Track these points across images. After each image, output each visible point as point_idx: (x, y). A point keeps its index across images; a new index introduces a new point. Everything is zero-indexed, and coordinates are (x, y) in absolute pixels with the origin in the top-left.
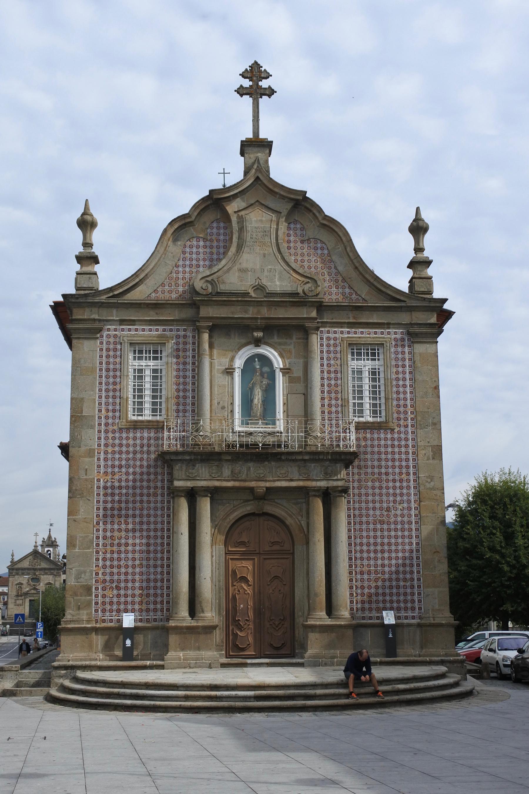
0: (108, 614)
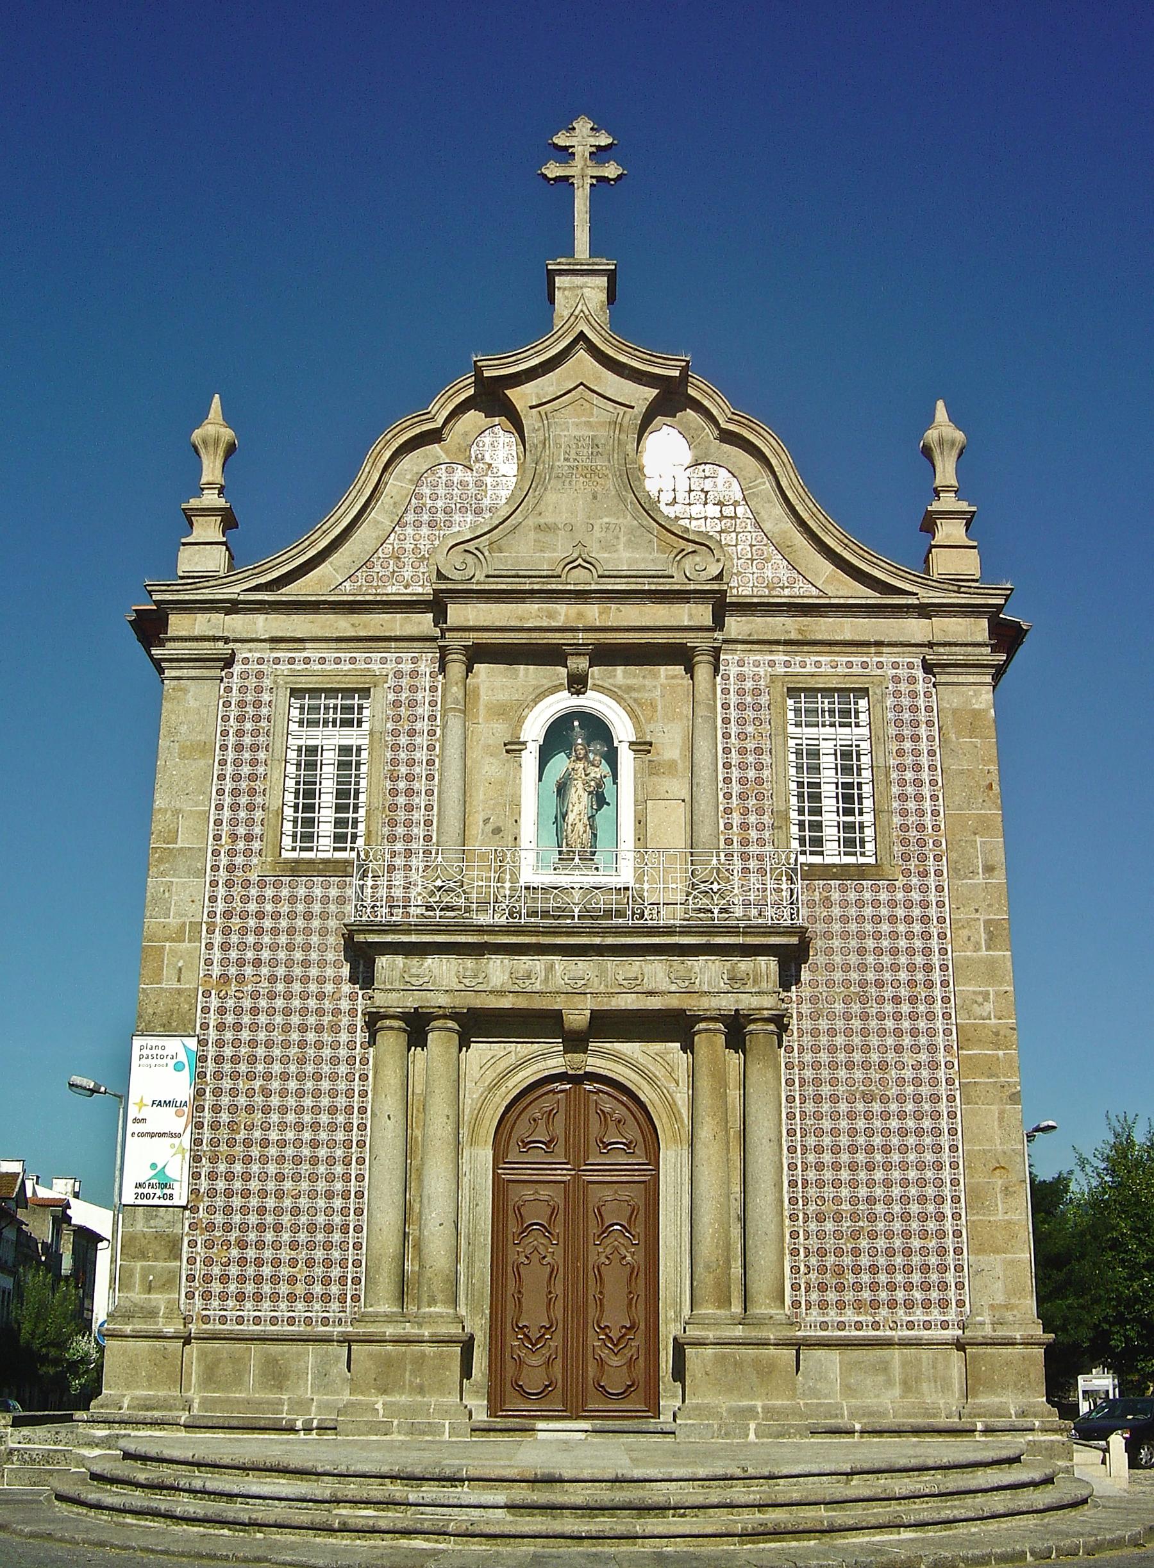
0: (215, 1303)
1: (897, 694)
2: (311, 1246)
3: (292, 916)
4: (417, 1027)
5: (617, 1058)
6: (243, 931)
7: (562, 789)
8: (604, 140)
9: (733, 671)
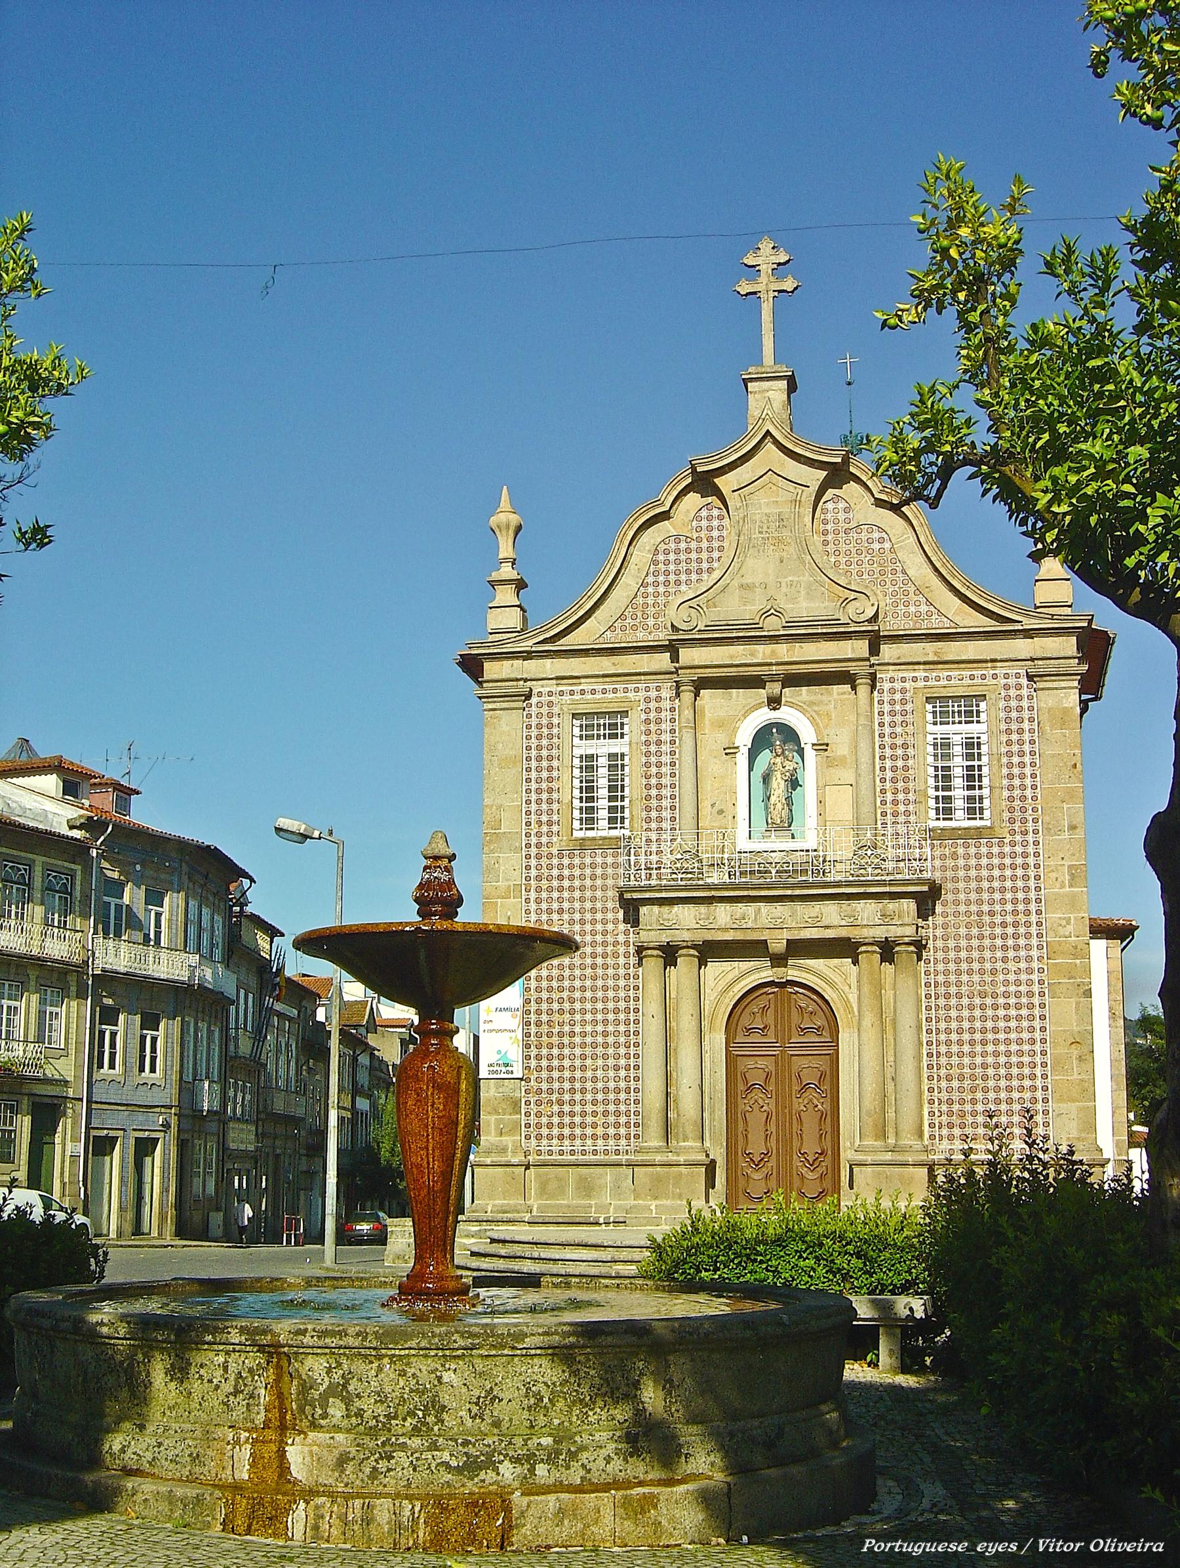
1: (1007, 698)
3: (582, 877)
4: (669, 953)
5: (808, 970)
6: (550, 889)
7: (766, 779)
8: (783, 258)
9: (887, 686)
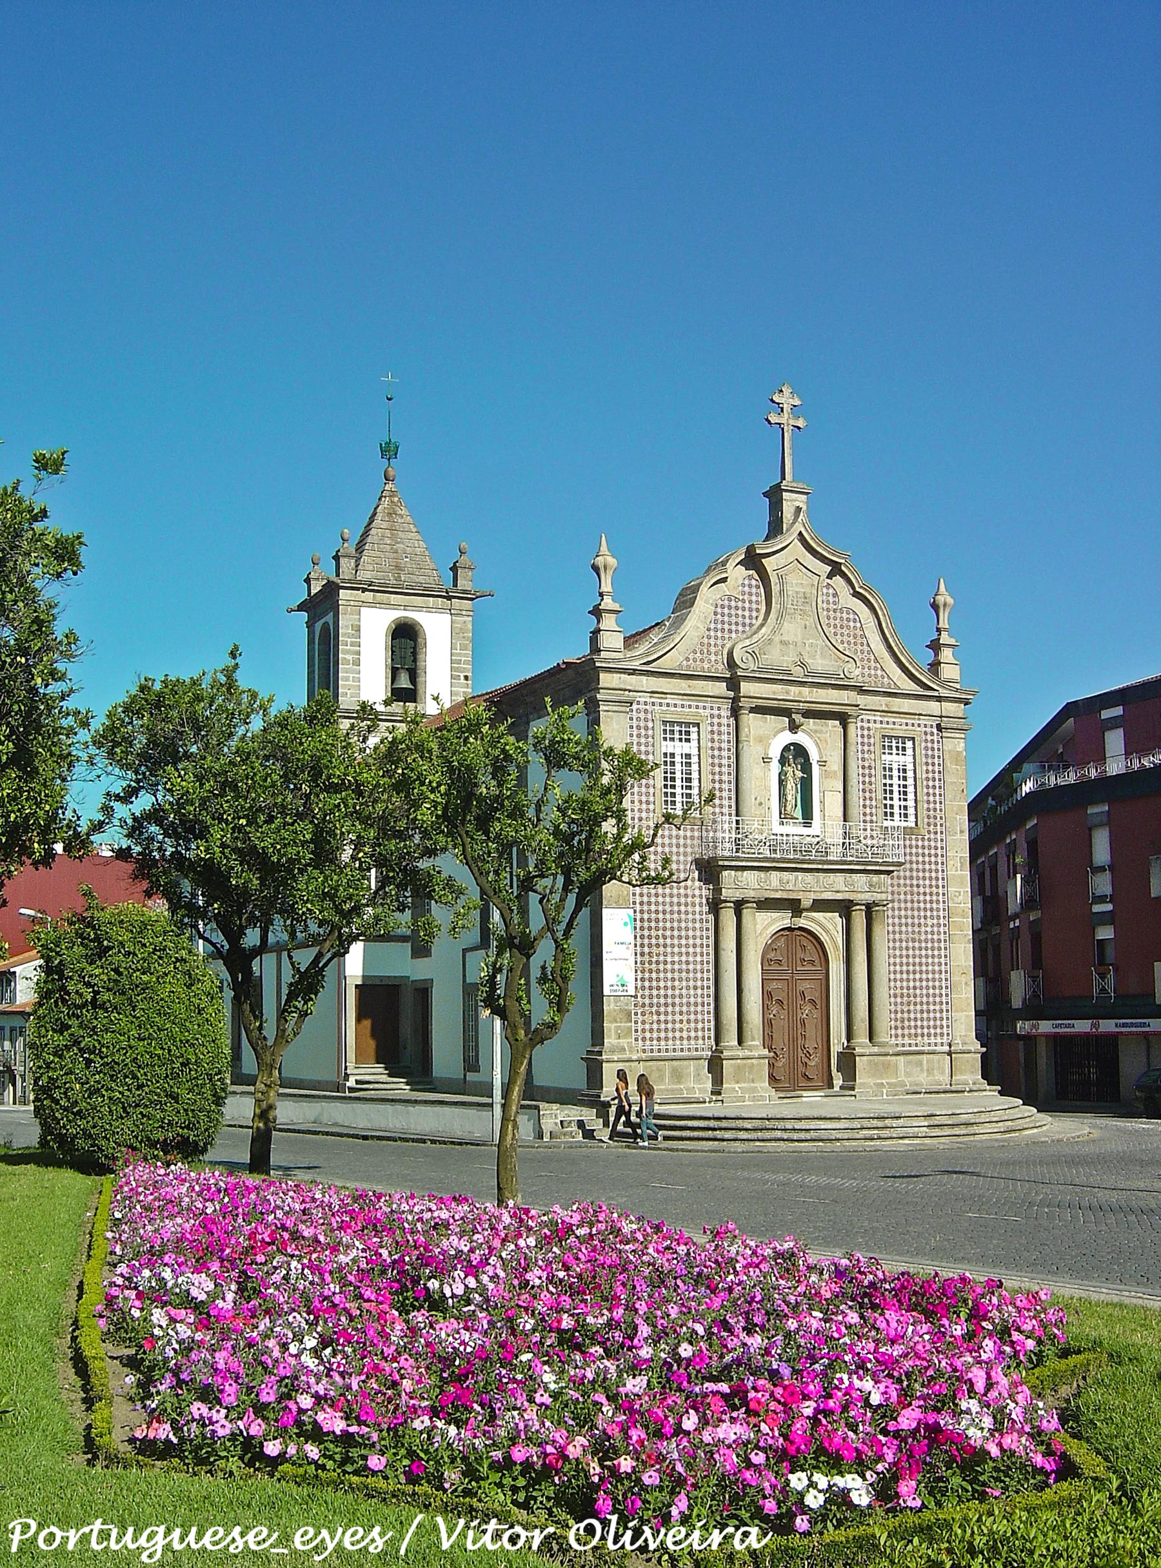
2: (688, 1013)
5: (813, 920)
